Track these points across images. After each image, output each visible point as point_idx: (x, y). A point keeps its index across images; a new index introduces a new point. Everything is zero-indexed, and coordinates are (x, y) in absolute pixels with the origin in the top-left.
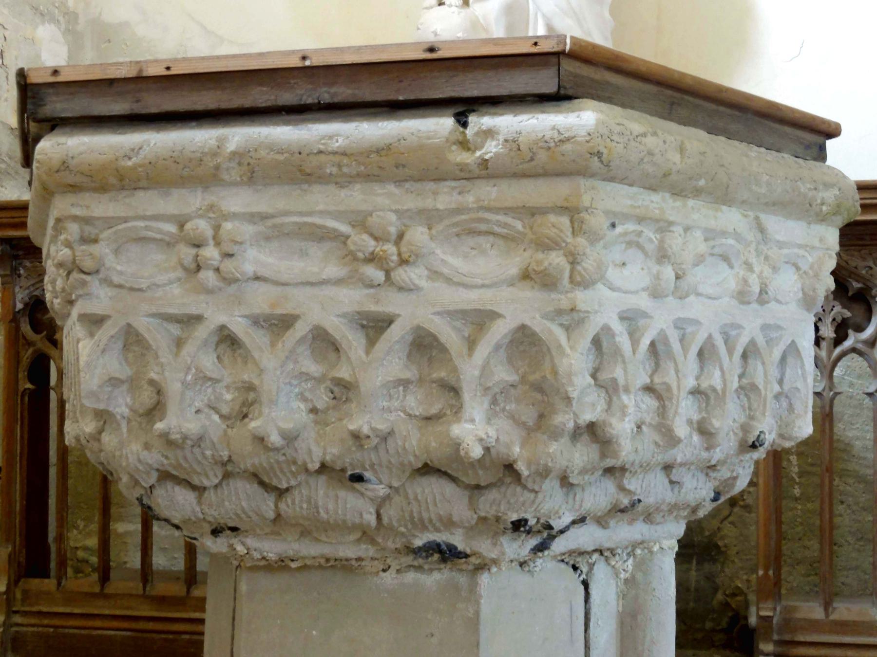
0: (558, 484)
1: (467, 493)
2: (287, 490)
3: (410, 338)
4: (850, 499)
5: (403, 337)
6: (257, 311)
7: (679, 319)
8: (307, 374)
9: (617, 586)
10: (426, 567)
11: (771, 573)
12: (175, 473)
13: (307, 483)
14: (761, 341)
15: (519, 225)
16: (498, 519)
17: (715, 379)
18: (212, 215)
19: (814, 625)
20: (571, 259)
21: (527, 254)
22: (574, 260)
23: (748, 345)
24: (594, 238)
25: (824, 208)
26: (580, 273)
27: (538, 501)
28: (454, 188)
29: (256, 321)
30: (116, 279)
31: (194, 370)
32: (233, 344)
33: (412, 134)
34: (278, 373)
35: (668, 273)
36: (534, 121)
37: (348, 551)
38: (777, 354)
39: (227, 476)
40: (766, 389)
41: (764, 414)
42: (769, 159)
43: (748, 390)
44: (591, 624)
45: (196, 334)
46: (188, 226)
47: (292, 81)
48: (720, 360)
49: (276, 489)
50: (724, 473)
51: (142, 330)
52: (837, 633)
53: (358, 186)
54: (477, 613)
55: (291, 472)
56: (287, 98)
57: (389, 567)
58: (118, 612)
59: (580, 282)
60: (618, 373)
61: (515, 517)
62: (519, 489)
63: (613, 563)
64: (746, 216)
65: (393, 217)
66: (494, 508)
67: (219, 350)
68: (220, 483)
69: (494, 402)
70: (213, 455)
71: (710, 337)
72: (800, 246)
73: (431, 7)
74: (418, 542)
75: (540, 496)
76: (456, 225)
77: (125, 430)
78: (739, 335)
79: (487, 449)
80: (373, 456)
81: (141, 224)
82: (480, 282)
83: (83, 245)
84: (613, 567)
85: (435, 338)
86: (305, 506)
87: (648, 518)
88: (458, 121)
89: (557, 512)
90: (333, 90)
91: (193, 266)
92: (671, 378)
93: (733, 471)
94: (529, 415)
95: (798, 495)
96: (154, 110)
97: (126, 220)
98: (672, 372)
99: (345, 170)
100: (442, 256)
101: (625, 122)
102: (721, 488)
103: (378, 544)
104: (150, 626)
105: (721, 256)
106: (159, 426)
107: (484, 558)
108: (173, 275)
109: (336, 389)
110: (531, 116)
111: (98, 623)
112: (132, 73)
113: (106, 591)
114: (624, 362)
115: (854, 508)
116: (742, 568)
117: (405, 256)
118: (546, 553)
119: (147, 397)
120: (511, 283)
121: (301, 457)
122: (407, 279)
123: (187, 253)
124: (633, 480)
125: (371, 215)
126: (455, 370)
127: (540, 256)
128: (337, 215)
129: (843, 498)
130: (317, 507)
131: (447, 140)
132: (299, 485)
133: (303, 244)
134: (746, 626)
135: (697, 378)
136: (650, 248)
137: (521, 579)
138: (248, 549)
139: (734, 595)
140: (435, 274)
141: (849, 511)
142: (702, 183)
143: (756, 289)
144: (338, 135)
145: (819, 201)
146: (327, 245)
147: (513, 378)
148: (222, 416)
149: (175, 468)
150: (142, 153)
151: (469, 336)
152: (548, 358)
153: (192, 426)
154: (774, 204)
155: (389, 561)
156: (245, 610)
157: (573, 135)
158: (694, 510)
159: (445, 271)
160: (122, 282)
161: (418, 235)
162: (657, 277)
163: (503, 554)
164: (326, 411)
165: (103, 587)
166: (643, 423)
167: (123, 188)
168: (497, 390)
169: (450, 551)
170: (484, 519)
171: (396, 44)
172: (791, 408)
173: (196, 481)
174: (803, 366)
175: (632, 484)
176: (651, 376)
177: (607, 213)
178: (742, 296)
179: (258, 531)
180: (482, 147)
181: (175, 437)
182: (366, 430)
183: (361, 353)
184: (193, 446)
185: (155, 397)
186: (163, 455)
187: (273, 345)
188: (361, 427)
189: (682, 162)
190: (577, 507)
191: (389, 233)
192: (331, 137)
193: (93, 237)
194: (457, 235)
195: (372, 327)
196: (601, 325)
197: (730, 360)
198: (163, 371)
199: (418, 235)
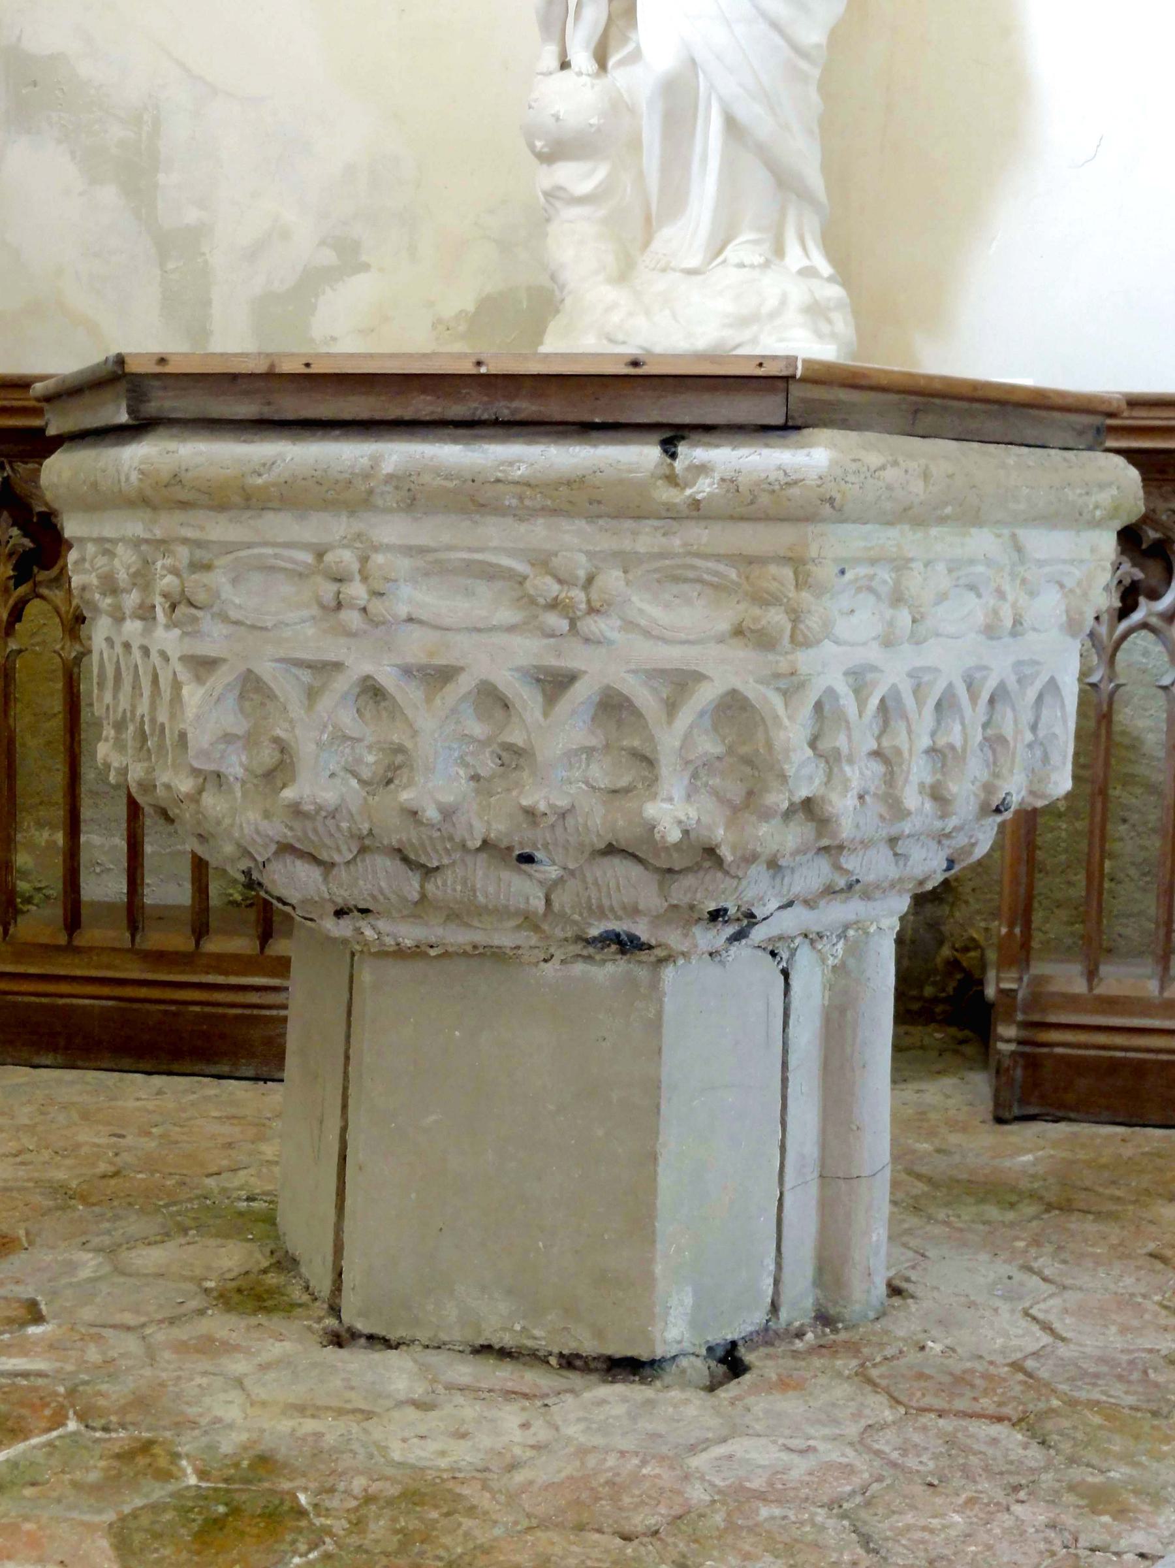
0: (765, 866)
1: (656, 877)
2: (438, 868)
3: (596, 699)
4: (1136, 816)
5: (590, 697)
6: (410, 660)
7: (915, 669)
8: (471, 737)
9: (823, 974)
10: (598, 957)
11: (1017, 930)
12: (298, 845)
13: (463, 861)
14: (1012, 684)
15: (733, 574)
16: (692, 907)
17: (954, 735)
18: (358, 545)
19: (1072, 1002)
20: (793, 616)
21: (742, 606)
22: (796, 616)
23: (996, 689)
24: (820, 591)
25: (1098, 513)
26: (802, 631)
27: (741, 888)
28: (656, 529)
29: (407, 671)
30: (234, 614)
31: (330, 728)
32: (376, 695)
33: (611, 465)
34: (436, 736)
35: (904, 617)
36: (755, 458)
37: (504, 939)
38: (1032, 694)
39: (363, 850)
40: (1015, 740)
41: (1011, 771)
42: (1031, 463)
43: (995, 742)
44: (791, 1022)
45: (335, 685)
46: (329, 558)
47: (464, 391)
48: (960, 710)
49: (423, 866)
50: (961, 840)
51: (266, 677)
52: (1104, 1012)
53: (540, 521)
54: (659, 1014)
55: (446, 849)
56: (457, 411)
57: (552, 956)
58: (94, 973)
59: (800, 641)
60: (841, 742)
61: (712, 907)
62: (719, 875)
63: (820, 947)
64: (999, 536)
65: (582, 559)
66: (689, 895)
67: (359, 701)
68: (355, 858)
69: (695, 776)
70: (349, 828)
71: (950, 685)
72: (1064, 562)
73: (551, 73)
74: (594, 932)
75: (744, 883)
76: (656, 570)
77: (239, 794)
78: (985, 678)
79: (686, 833)
80: (548, 836)
81: (269, 551)
82: (683, 636)
83: (194, 573)
84: (819, 951)
85: (628, 699)
86: (459, 888)
87: (867, 896)
88: (666, 451)
89: (761, 899)
90: (515, 404)
91: (333, 604)
92: (902, 740)
93: (971, 837)
94: (735, 791)
95: (1063, 809)
96: (290, 416)
97: (249, 546)
98: (904, 734)
99: (527, 502)
100: (639, 604)
101: (862, 454)
102: (955, 856)
103: (543, 932)
104: (143, 992)
105: (967, 586)
106: (289, 794)
107: (671, 949)
108: (305, 613)
109: (504, 754)
110: (752, 450)
111: (64, 988)
112: (262, 368)
113: (76, 943)
114: (848, 728)
115: (1140, 829)
116: (979, 912)
117: (596, 605)
118: (744, 942)
119: (267, 756)
120: (721, 640)
121: (460, 833)
122: (597, 631)
123: (328, 590)
124: (853, 857)
125: (556, 555)
126: (651, 738)
127: (757, 611)
128: (512, 553)
129: (1126, 814)
130: (474, 890)
131: (652, 475)
132: (454, 863)
133: (469, 582)
134: (982, 992)
135: (933, 734)
136: (884, 590)
137: (711, 972)
138: (379, 933)
139: (966, 949)
140: (629, 625)
141: (1133, 834)
142: (948, 510)
143: (1008, 623)
144: (519, 461)
145: (1091, 507)
146: (499, 584)
147: (716, 749)
148: (361, 781)
149: (299, 840)
150: (276, 470)
151: (668, 698)
152: (761, 729)
153: (329, 796)
154: (1034, 520)
155: (552, 950)
156: (367, 1005)
157: (801, 477)
158: (921, 883)
159: (643, 622)
160: (241, 618)
161: (612, 580)
162: (891, 624)
163: (696, 946)
164: (489, 780)
165: (70, 936)
166: (867, 792)
167: (248, 508)
168: (699, 763)
169: (632, 942)
170: (675, 907)
171: (592, 354)
172: (1046, 759)
173: (324, 856)
174: (1063, 706)
175: (850, 862)
176: (878, 738)
177: (835, 560)
178: (990, 631)
179: (395, 914)
180: (694, 484)
181: (308, 807)
182: (542, 807)
183: (538, 714)
184: (325, 817)
185: (277, 755)
186: (287, 826)
187: (429, 700)
188: (537, 802)
189: (925, 491)
190: (785, 891)
191: (577, 578)
192: (511, 464)
193: (205, 561)
194: (658, 581)
195: (550, 682)
196: (823, 688)
197: (974, 710)
198: (293, 728)
199: (612, 580)
